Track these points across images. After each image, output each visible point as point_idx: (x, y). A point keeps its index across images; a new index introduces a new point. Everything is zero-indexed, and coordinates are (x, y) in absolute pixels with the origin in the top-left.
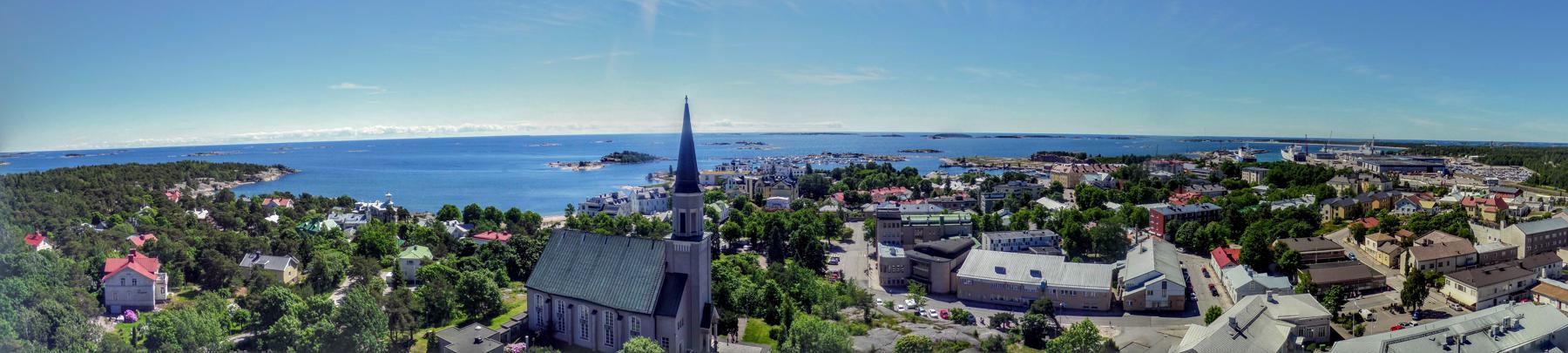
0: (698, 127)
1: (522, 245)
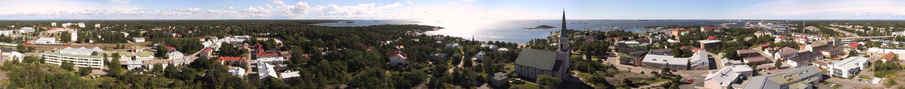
0: (566, 18)
1: (513, 53)
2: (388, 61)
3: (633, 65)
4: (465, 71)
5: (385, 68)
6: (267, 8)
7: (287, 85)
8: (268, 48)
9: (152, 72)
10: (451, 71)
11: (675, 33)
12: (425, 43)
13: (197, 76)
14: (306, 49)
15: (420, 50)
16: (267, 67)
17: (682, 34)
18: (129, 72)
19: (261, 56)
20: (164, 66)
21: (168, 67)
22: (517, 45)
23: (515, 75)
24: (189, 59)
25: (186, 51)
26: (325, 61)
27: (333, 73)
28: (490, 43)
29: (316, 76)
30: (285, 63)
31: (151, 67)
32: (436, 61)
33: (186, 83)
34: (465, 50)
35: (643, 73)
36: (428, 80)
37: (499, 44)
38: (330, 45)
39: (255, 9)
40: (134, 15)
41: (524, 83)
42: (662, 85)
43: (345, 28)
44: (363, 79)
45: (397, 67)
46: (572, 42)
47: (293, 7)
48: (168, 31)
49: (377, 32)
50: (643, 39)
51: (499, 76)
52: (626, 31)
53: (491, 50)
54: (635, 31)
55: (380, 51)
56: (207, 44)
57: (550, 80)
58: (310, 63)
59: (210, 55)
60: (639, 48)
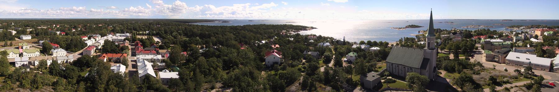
0: (434, 18)
1: (384, 51)
2: (263, 60)
3: (498, 62)
4: (335, 71)
5: (260, 69)
6: (147, 8)
7: (165, 87)
8: (147, 46)
9: (38, 69)
10: (322, 69)
11: (538, 33)
12: (299, 42)
13: (80, 76)
14: (185, 46)
15: (295, 49)
16: (146, 64)
17: (546, 34)
18: (17, 69)
19: (141, 53)
20: (49, 63)
21: (52, 64)
22: (387, 44)
23: (387, 73)
24: (73, 57)
25: (69, 48)
26: (202, 59)
27: (209, 70)
28: (362, 43)
29: (194, 74)
30: (163, 61)
31: (37, 63)
32: (309, 59)
33: (69, 83)
34: (336, 49)
35: (506, 70)
36: (302, 78)
37: (370, 44)
38: (207, 43)
39: (135, 9)
40: (21, 14)
41: (395, 82)
42: (525, 86)
43: (221, 27)
44: (237, 78)
45: (272, 67)
46: (439, 41)
47: (170, 6)
48: (52, 29)
49: (252, 31)
50: (508, 38)
51: (371, 77)
52: (492, 30)
53: (363, 50)
54: (500, 30)
55: (254, 50)
56: (90, 43)
57: (419, 78)
58: (188, 61)
59: (93, 53)
60: (503, 46)
